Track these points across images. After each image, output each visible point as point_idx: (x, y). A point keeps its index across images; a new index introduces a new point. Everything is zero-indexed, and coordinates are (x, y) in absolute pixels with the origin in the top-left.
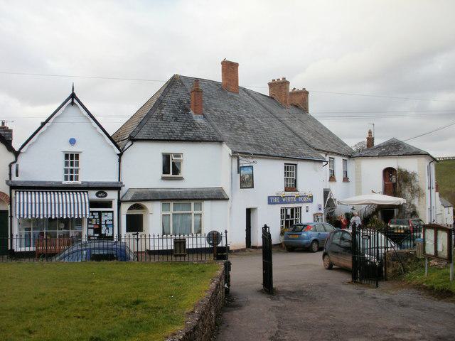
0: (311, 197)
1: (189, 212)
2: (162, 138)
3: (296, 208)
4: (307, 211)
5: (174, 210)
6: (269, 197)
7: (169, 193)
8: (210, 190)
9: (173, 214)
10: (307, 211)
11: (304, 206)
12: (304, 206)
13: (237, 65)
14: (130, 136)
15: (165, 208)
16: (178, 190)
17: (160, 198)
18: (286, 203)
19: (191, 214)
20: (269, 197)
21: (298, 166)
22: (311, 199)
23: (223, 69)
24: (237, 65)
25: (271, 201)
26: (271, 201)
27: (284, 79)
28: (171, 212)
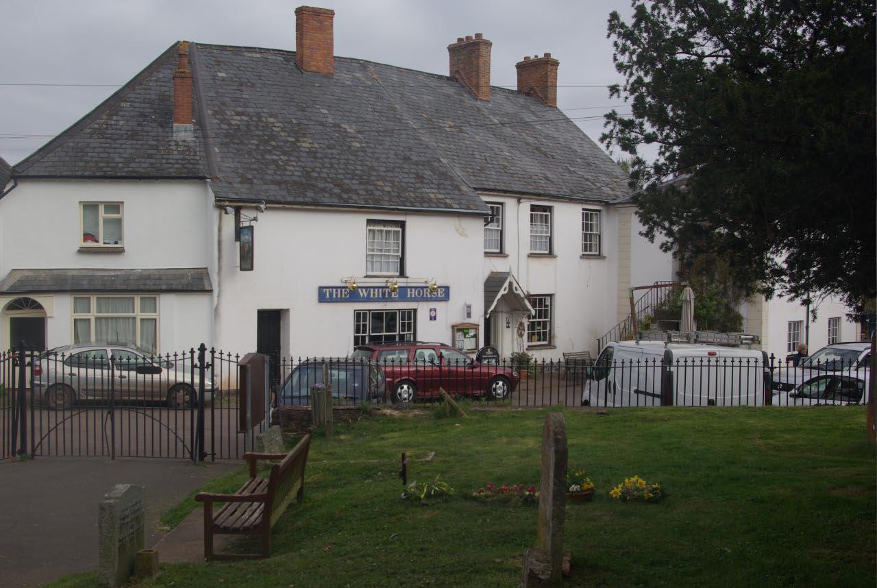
0: (447, 288)
1: (131, 315)
2: (79, 173)
3: (403, 312)
4: (433, 318)
5: (99, 311)
6: (321, 288)
7: (91, 279)
8: (179, 273)
9: (97, 319)
10: (433, 318)
11: (423, 310)
12: (423, 310)
13: (330, 14)
14: (646, 330)
15: (79, 306)
16: (112, 273)
17: (68, 287)
18: (368, 299)
19: (134, 318)
20: (321, 288)
21: (129, 216)
22: (444, 294)
23: (309, 7)
24: (330, 14)
25: (326, 295)
26: (326, 295)
27: (478, 36)
28: (92, 315)
